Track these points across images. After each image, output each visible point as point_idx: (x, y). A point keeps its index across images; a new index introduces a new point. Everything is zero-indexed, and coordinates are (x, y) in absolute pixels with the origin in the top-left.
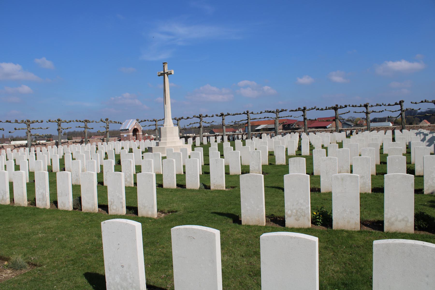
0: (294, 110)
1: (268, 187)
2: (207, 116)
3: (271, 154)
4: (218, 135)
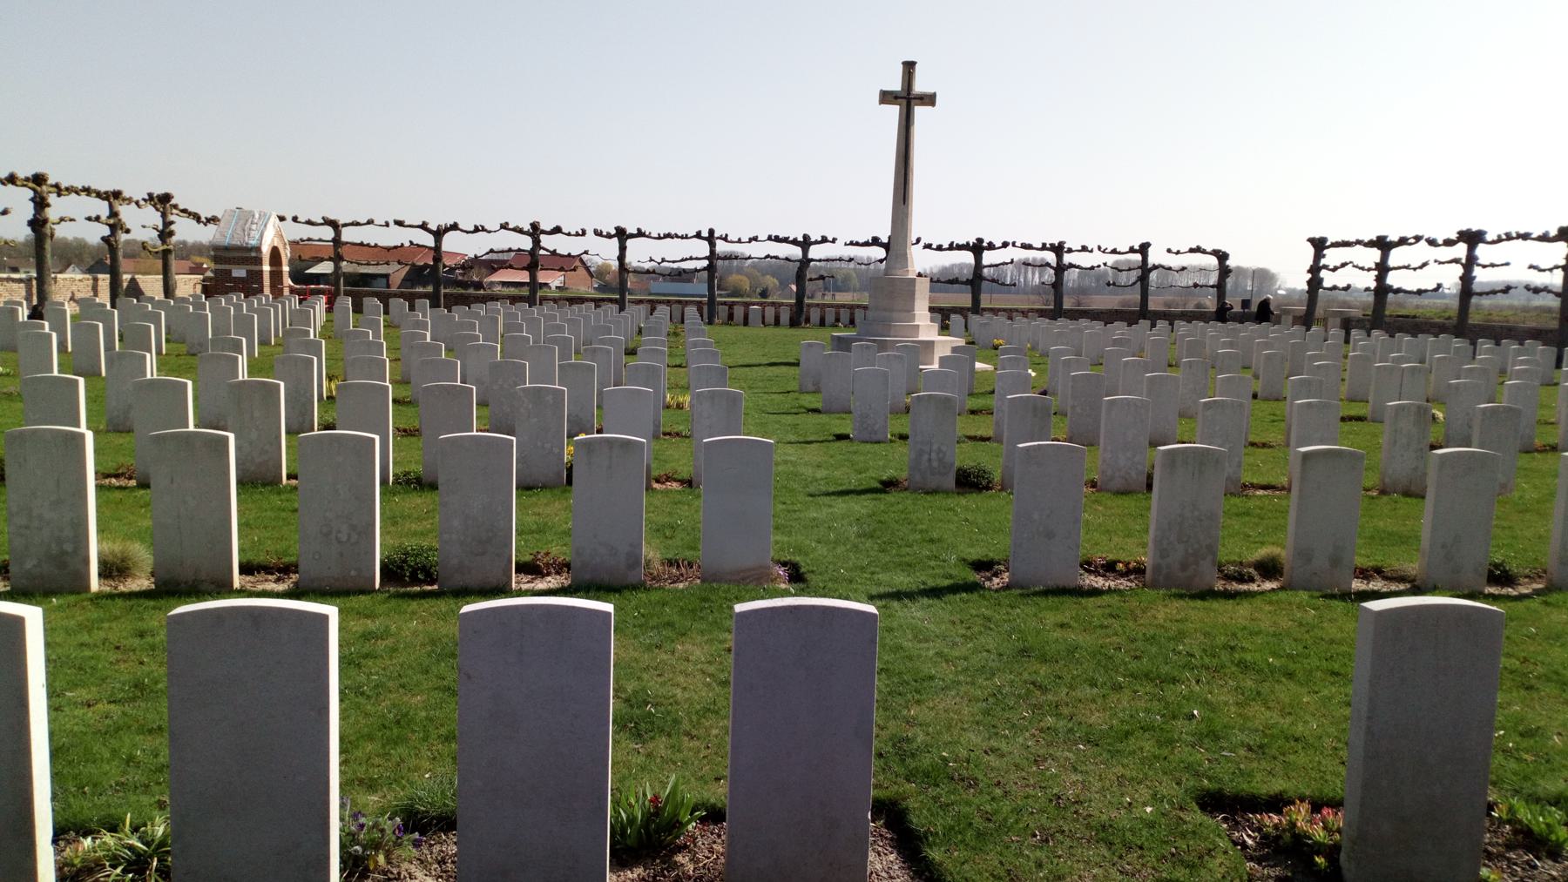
2: (557, 230)
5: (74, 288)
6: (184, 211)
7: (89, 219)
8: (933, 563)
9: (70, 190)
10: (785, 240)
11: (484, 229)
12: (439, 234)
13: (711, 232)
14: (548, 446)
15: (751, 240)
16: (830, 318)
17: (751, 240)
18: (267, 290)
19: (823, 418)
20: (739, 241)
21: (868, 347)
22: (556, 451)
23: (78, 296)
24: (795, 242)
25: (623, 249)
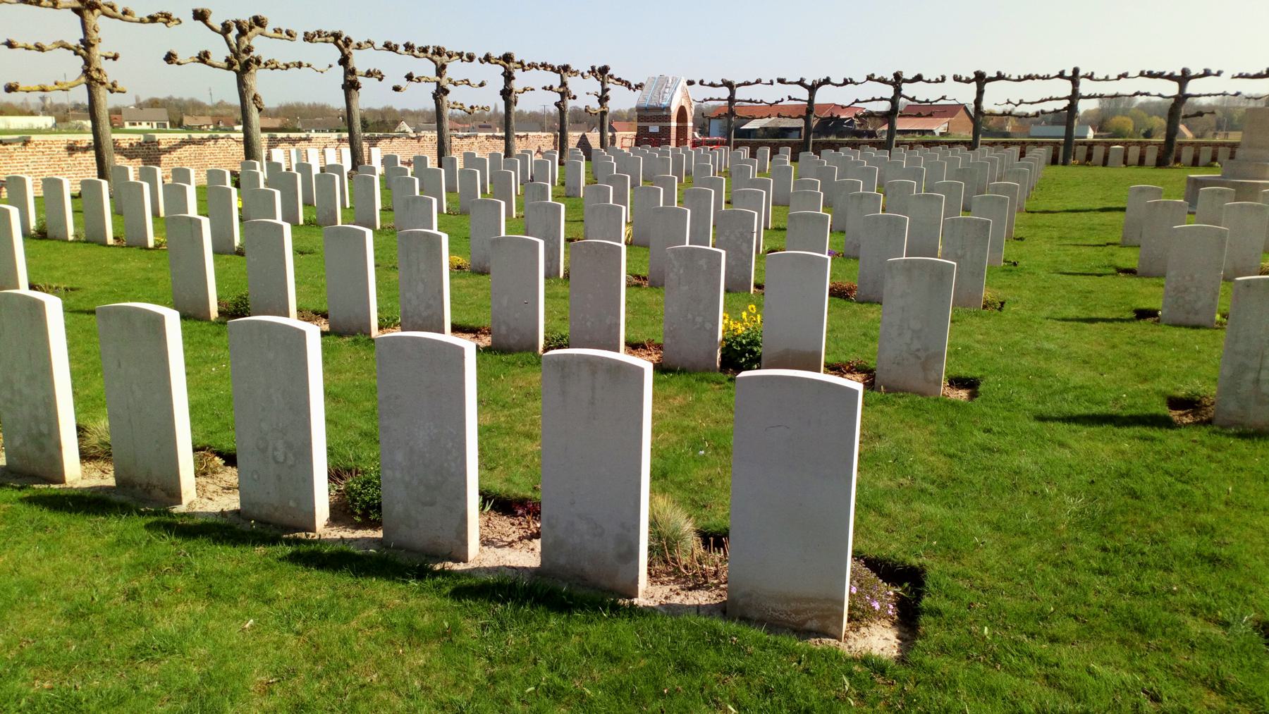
0: (1252, 73)
1: (302, 253)
2: (918, 78)
3: (575, 98)
4: (762, 144)
5: (540, 143)
6: (618, 80)
7: (545, 88)
8: (1195, 627)
9: (531, 66)
10: (1160, 75)
11: (852, 82)
12: (812, 89)
13: (1076, 71)
14: (699, 319)
15: (1119, 77)
16: (1205, 155)
17: (1119, 77)
18: (673, 142)
19: (1133, 282)
20: (1107, 79)
21: (1221, 193)
22: (708, 326)
23: (544, 149)
24: (1171, 77)
25: (980, 93)
